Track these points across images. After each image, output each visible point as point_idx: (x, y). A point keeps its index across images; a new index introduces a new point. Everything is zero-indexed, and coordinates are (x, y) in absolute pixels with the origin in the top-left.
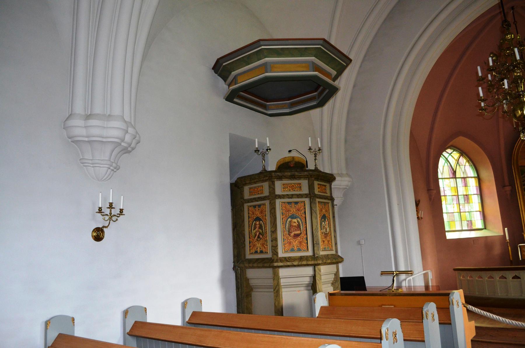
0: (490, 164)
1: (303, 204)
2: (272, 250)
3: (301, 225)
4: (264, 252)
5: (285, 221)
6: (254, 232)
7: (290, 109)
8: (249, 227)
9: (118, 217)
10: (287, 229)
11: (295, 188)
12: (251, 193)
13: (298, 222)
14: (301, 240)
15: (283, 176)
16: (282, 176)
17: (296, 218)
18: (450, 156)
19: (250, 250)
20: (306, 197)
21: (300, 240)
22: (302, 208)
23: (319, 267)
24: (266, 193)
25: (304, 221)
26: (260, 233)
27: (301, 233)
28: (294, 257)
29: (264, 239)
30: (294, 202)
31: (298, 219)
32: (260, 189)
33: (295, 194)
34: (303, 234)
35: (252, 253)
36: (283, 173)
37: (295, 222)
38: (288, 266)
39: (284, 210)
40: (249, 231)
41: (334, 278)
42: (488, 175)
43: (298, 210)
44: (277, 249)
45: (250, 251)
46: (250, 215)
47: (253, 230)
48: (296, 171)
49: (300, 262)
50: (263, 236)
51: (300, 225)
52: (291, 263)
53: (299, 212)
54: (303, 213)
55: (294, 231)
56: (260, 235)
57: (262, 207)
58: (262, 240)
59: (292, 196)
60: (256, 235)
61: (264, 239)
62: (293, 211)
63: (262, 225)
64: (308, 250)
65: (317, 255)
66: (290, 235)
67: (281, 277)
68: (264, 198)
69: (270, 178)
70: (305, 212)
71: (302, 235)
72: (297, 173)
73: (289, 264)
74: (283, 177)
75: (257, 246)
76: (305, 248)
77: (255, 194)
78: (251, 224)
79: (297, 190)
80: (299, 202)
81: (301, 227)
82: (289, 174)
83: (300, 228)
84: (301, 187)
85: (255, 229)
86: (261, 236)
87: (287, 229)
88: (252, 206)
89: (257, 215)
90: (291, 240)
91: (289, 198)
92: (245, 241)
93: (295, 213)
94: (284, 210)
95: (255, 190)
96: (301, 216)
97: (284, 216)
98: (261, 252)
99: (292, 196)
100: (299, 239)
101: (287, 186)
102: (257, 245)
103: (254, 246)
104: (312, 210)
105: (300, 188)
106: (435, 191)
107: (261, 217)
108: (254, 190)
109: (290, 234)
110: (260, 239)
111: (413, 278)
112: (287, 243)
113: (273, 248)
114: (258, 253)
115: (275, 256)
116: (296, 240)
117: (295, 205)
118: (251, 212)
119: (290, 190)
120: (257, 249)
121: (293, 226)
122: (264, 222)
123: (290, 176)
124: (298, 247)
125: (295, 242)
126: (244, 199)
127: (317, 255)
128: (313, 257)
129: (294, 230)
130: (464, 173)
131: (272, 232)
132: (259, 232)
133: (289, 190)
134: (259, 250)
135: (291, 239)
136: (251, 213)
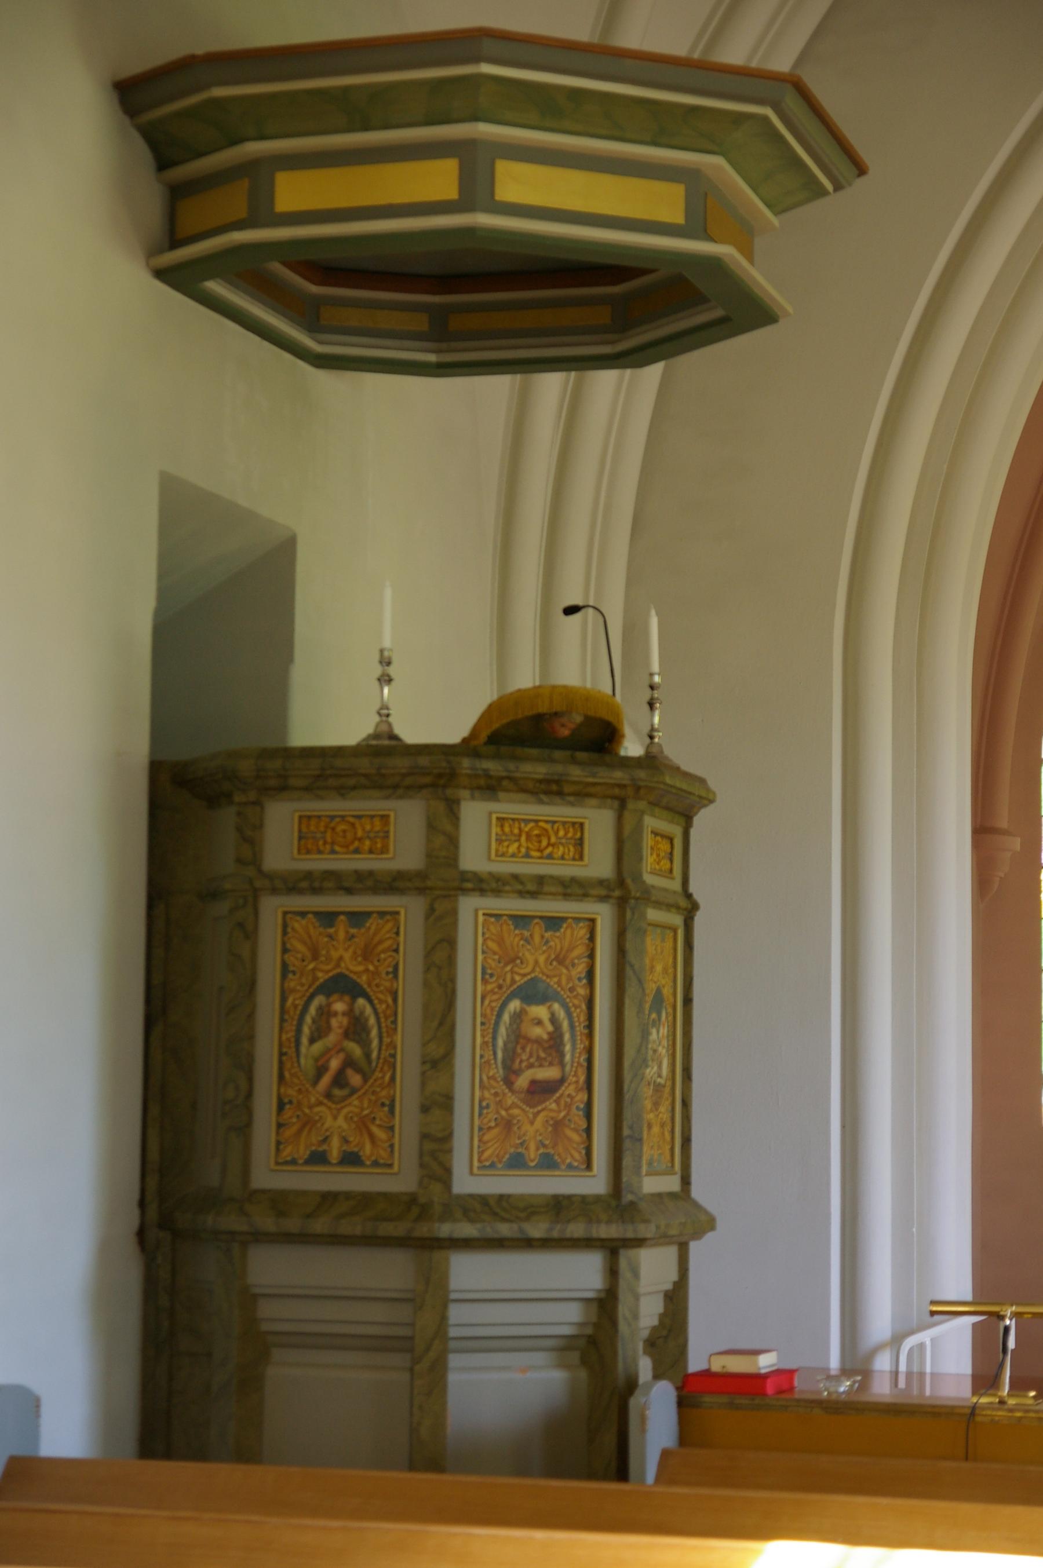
1: (582, 932)
2: (421, 1155)
3: (567, 1037)
4: (368, 1163)
5: (492, 1009)
6: (310, 1051)
7: (444, 345)
8: (282, 1020)
10: (500, 1055)
11: (553, 845)
12: (306, 842)
13: (553, 1020)
14: (563, 1114)
15: (509, 778)
16: (501, 779)
17: (543, 998)
19: (278, 1143)
20: (603, 899)
21: (552, 1114)
23: (632, 1253)
25: (580, 1016)
26: (349, 1063)
27: (562, 1081)
28: (522, 1197)
29: (374, 1093)
30: (541, 917)
31: (556, 1006)
32: (368, 827)
33: (552, 877)
34: (572, 1087)
35: (293, 1162)
36: (511, 766)
37: (539, 1023)
38: (498, 1244)
39: (495, 953)
40: (281, 1045)
41: (662, 1317)
43: (557, 958)
44: (450, 1151)
45: (278, 1150)
46: (290, 958)
47: (305, 1040)
48: (574, 761)
49: (559, 1227)
50: (365, 1080)
51: (561, 1036)
52: (515, 1226)
53: (564, 971)
54: (580, 979)
55: (531, 1066)
56: (350, 1072)
57: (372, 923)
58: (360, 1098)
60: (321, 1071)
61: (374, 1093)
62: (536, 962)
63: (367, 1020)
64: (589, 1166)
66: (512, 1083)
67: (453, 1296)
68: (394, 879)
69: (442, 782)
71: (569, 1089)
72: (576, 773)
73: (505, 1230)
74: (505, 783)
75: (326, 1126)
76: (577, 1155)
77: (333, 852)
78: (296, 1007)
79: (563, 858)
80: (563, 919)
81: (568, 1048)
82: (540, 770)
83: (562, 1055)
84: (580, 843)
85: (320, 1037)
86: (355, 1079)
87: (500, 1055)
88: (307, 913)
89: (338, 966)
90: (516, 1111)
91: (522, 894)
92: (249, 1095)
93: (543, 974)
94: (495, 953)
95: (333, 829)
96: (572, 990)
97: (489, 987)
98: (351, 1159)
100: (554, 1106)
101: (516, 831)
102: (329, 1122)
103: (308, 1123)
104: (628, 969)
105: (575, 845)
106: (1016, 844)
107: (363, 980)
108: (326, 827)
109: (513, 1077)
110: (345, 1092)
111: (932, 1340)
112: (497, 1125)
113: (429, 1146)
114: (329, 1163)
115: (436, 1188)
116: (539, 1112)
117: (548, 935)
118: (304, 943)
119: (527, 855)
120: (325, 1140)
121: (528, 1040)
122: (381, 1008)
123: (541, 781)
124: (545, 1146)
125: (532, 1123)
126: (260, 871)
127: (632, 1193)
128: (614, 1203)
129: (532, 1060)
131: (428, 1066)
132: (342, 1056)
133: (523, 850)
135: (514, 1105)
136: (300, 947)
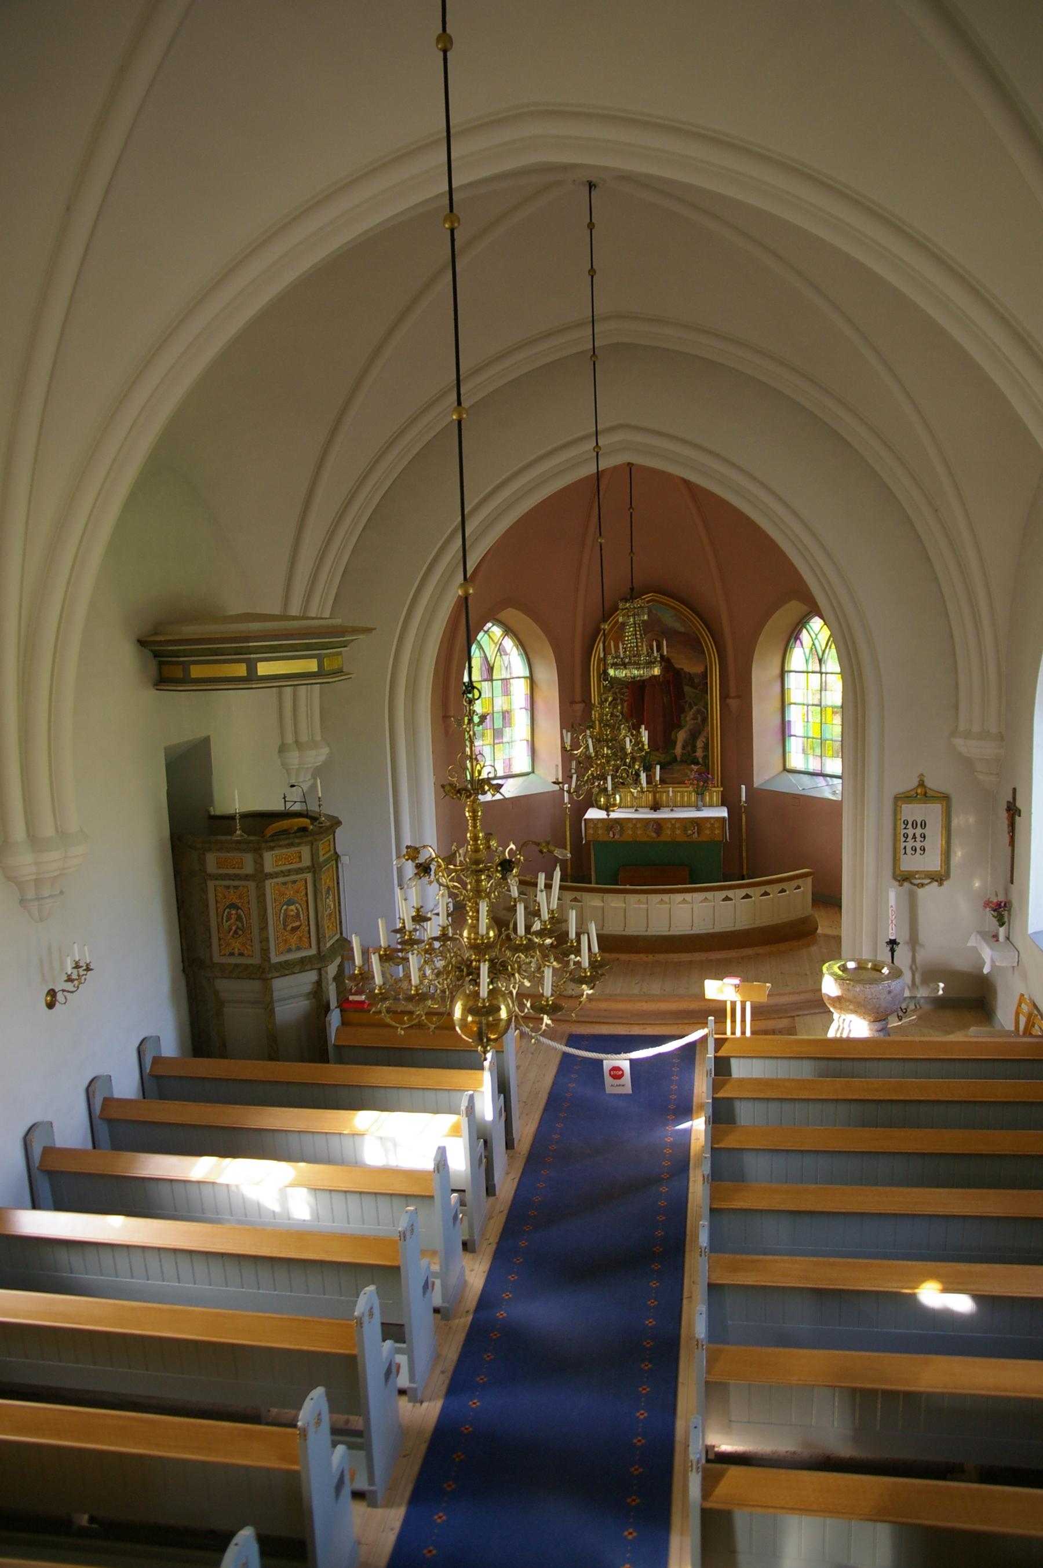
0: (552, 655)
6: (226, 925)
9: (86, 975)
12: (219, 865)
13: (297, 909)
17: (293, 903)
18: (486, 635)
22: (302, 888)
24: (249, 869)
25: (305, 906)
26: (238, 928)
27: (301, 925)
31: (297, 905)
35: (225, 955)
37: (293, 910)
42: (549, 677)
46: (219, 899)
47: (224, 921)
50: (243, 932)
59: (289, 872)
65: (323, 954)
70: (306, 894)
71: (303, 927)
86: (240, 932)
99: (289, 872)
103: (228, 945)
107: (240, 905)
122: (246, 913)
130: (507, 668)
134: (236, 951)
136: (220, 895)
